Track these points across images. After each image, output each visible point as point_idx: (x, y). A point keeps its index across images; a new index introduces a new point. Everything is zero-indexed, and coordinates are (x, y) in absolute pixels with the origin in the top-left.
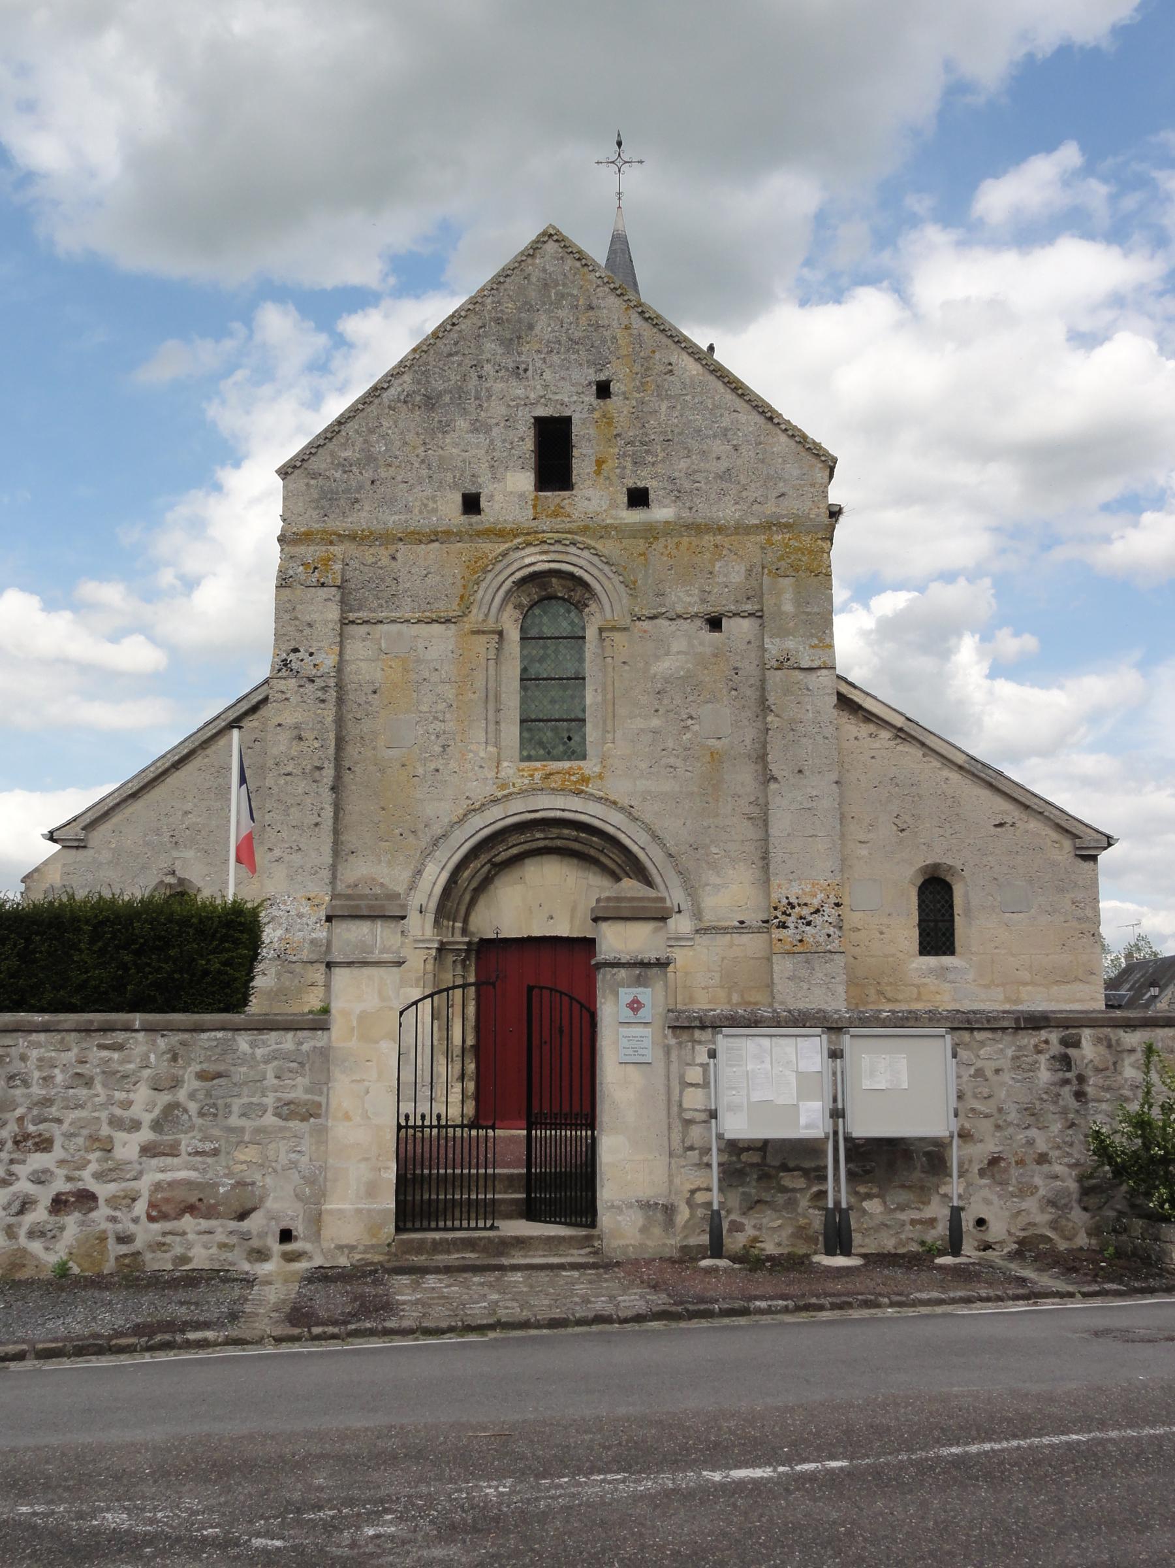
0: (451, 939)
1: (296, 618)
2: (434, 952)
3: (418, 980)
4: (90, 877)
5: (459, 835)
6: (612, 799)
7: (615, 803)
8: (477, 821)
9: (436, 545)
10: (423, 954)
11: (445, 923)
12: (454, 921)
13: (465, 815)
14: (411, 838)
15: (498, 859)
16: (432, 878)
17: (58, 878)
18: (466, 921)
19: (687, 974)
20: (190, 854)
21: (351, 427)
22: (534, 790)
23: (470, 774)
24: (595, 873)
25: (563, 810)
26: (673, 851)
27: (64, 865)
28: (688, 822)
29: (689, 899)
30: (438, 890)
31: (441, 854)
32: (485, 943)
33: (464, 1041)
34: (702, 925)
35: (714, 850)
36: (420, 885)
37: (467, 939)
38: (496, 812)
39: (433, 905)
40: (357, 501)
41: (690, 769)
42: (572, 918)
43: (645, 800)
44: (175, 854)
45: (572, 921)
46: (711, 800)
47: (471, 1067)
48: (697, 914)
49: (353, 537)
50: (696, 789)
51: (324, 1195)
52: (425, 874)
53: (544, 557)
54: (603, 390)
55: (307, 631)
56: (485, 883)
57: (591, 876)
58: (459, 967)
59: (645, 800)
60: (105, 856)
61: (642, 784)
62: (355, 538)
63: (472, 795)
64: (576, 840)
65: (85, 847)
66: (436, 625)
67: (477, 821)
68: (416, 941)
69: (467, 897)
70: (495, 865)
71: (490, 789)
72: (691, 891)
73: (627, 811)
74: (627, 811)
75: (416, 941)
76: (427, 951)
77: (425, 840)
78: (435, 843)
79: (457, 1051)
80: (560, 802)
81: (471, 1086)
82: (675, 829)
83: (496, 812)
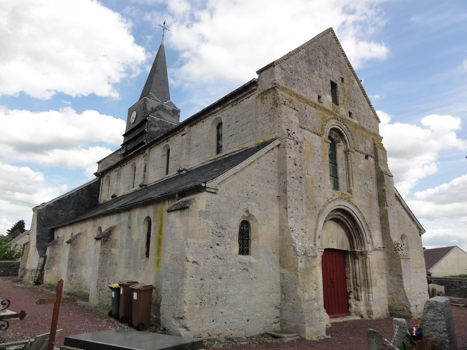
1: (287, 118)
4: (217, 208)
9: (314, 108)
17: (204, 207)
20: (253, 204)
21: (292, 58)
27: (207, 201)
38: (352, 207)
40: (294, 84)
44: (249, 203)
49: (297, 96)
51: (99, 272)
53: (336, 124)
54: (342, 79)
55: (291, 124)
60: (223, 199)
62: (297, 96)
65: (215, 193)
66: (316, 135)
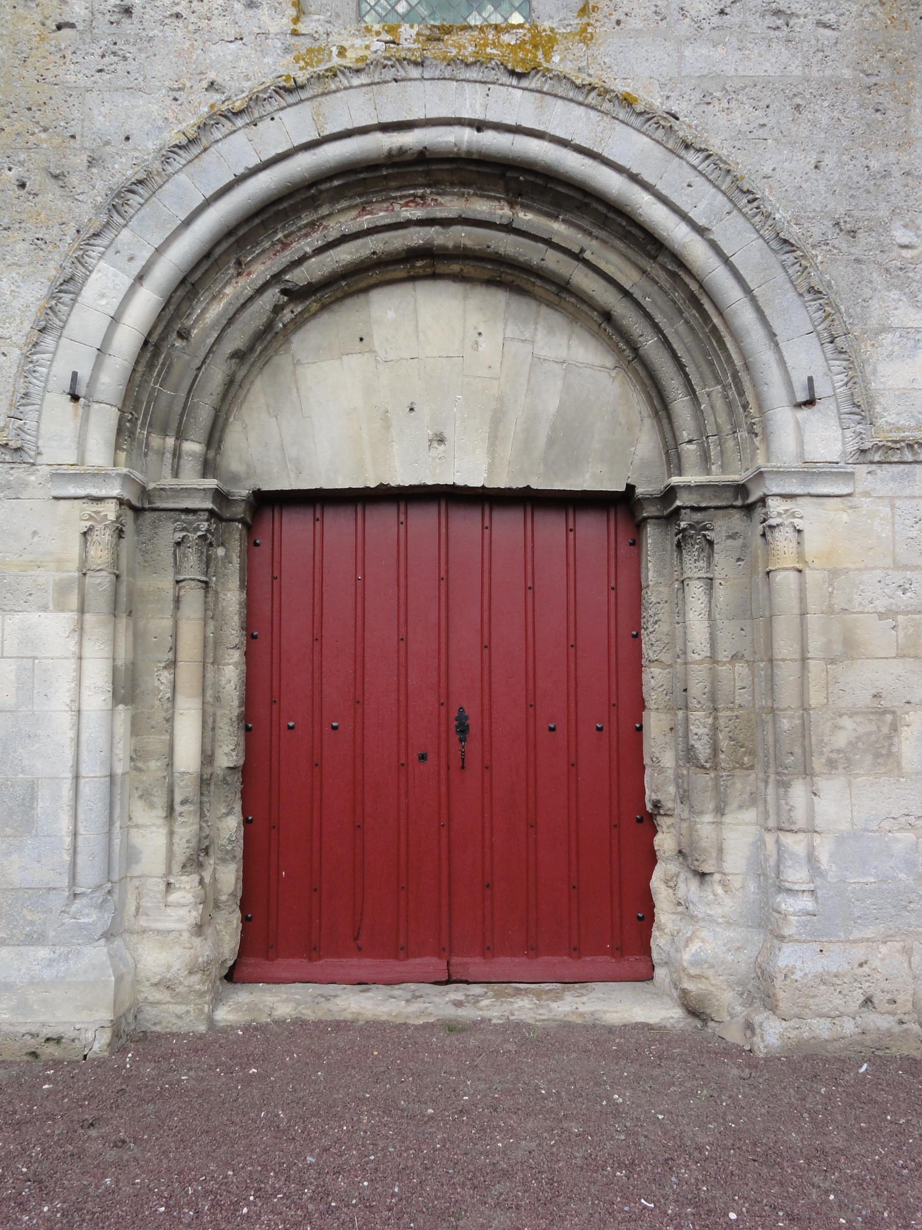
0: (168, 481)
2: (110, 511)
3: (62, 589)
5: (188, 186)
6: (620, 87)
7: (627, 101)
8: (238, 149)
10: (75, 517)
11: (156, 441)
12: (180, 436)
13: (203, 127)
14: (51, 195)
15: (300, 277)
16: (111, 305)
18: (214, 438)
19: (835, 573)
22: (396, 65)
23: (218, 23)
24: (551, 331)
25: (480, 126)
26: (793, 232)
28: (829, 160)
29: (838, 365)
30: (127, 339)
31: (136, 239)
32: (268, 502)
33: (207, 758)
34: (881, 438)
35: (901, 235)
36: (74, 322)
37: (211, 483)
38: (292, 125)
39: (111, 380)
41: (831, 18)
42: (494, 438)
43: (706, 99)
45: (492, 451)
46: (886, 100)
47: (230, 825)
48: (860, 408)
50: (847, 73)
52: (89, 293)
56: (267, 341)
57: (541, 335)
58: (192, 559)
59: (706, 99)
61: (700, 57)
63: (221, 78)
64: (508, 228)
67: (238, 149)
68: (58, 476)
69: (217, 374)
70: (294, 294)
71: (274, 65)
72: (837, 340)
73: (659, 123)
74: (659, 123)
75: (58, 476)
76: (91, 508)
77: (93, 193)
78: (118, 204)
79: (184, 789)
80: (471, 101)
81: (229, 877)
82: (787, 171)
83: (292, 125)
